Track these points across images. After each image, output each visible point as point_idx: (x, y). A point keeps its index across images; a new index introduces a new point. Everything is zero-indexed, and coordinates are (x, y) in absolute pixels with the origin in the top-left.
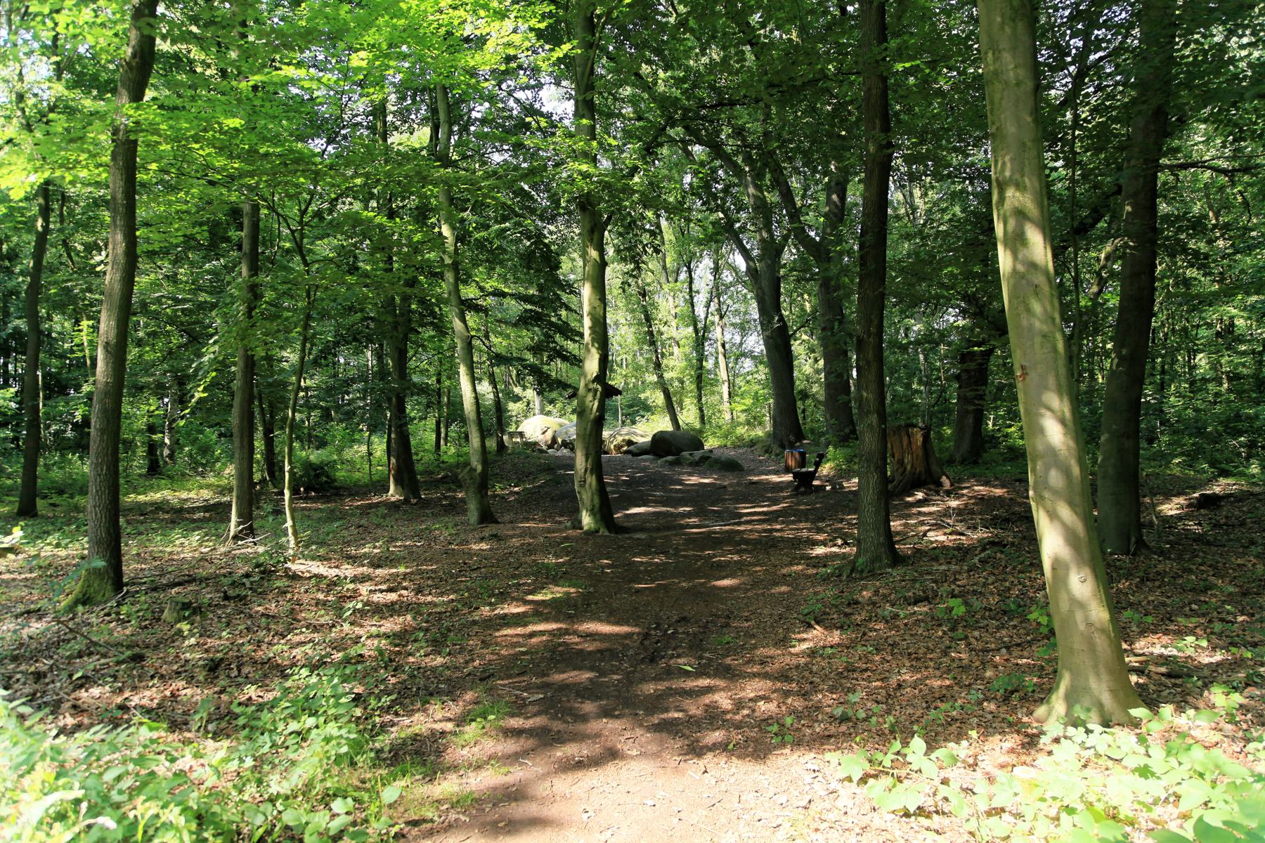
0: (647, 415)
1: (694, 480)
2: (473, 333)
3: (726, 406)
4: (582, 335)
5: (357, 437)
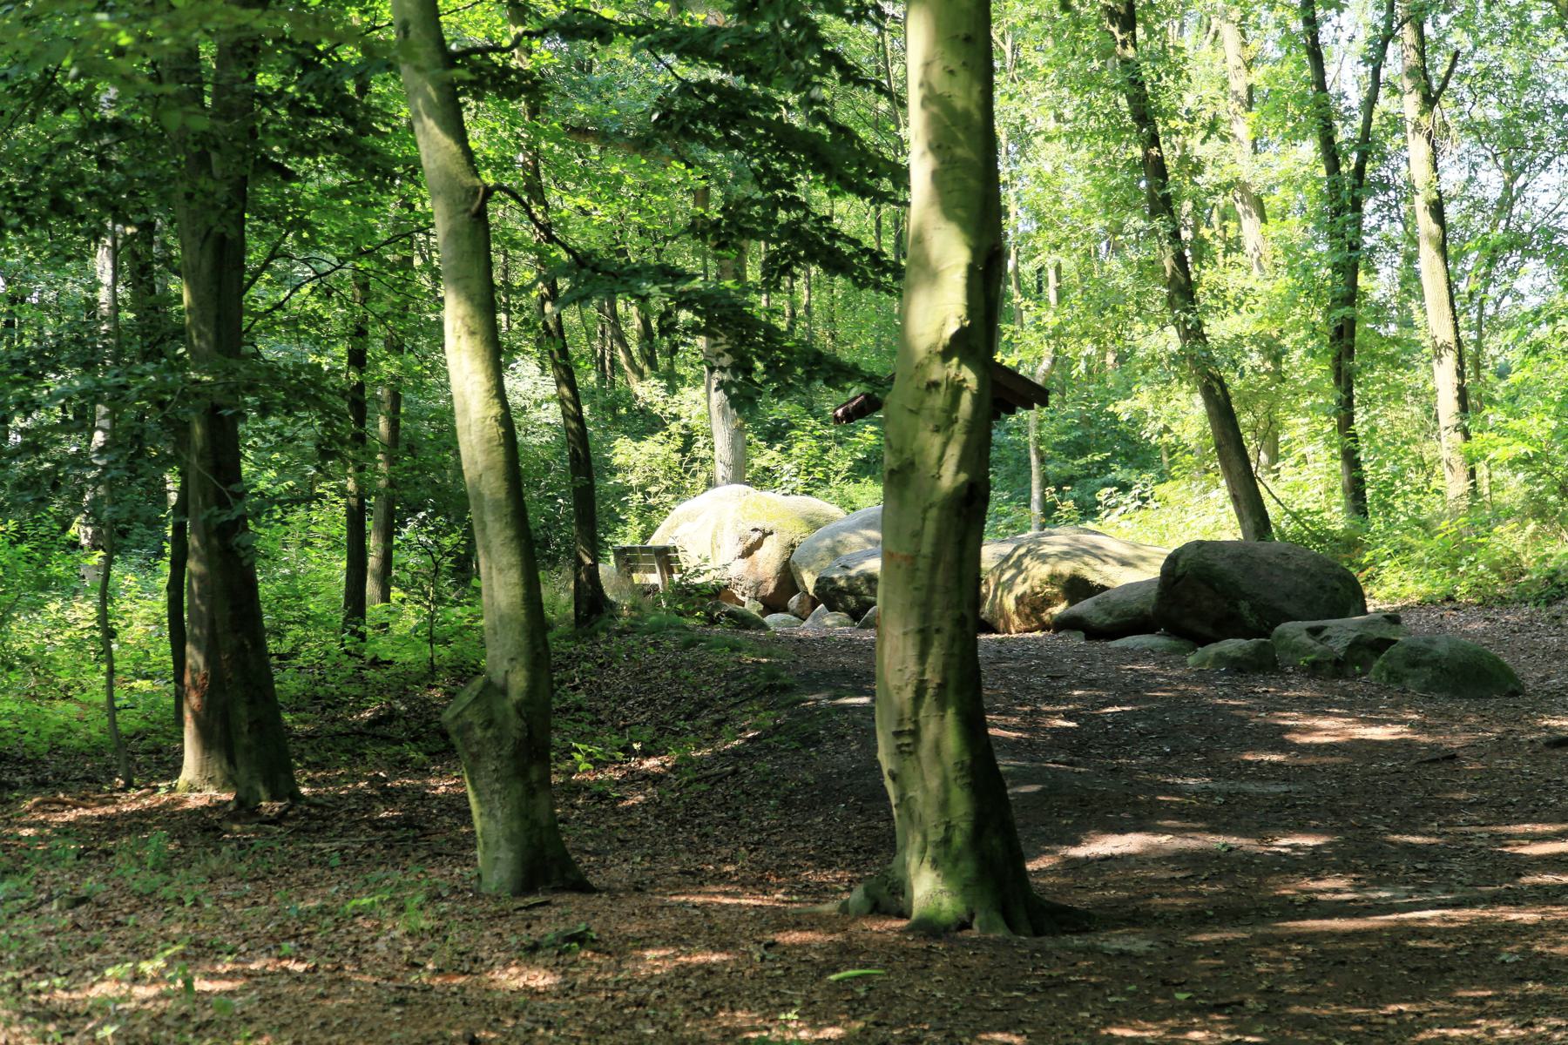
0: (1142, 480)
1: (1329, 729)
2: (488, 178)
3: (1448, 445)
4: (901, 176)
5: (56, 570)
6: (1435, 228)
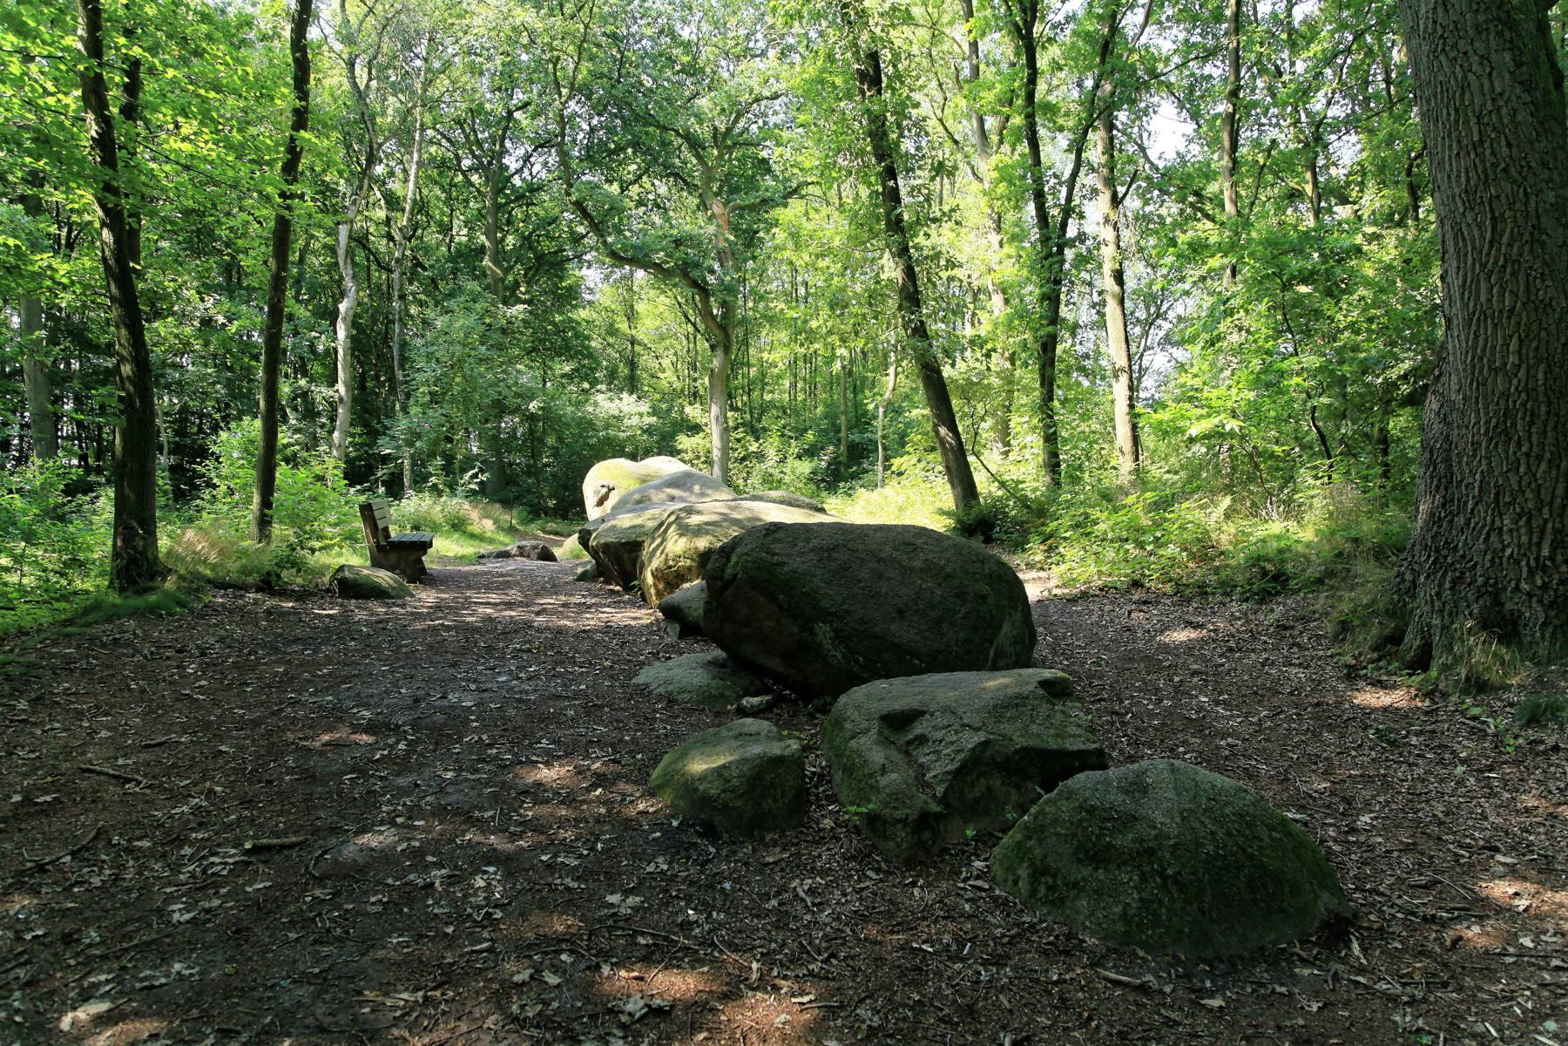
6: (1117, 289)
